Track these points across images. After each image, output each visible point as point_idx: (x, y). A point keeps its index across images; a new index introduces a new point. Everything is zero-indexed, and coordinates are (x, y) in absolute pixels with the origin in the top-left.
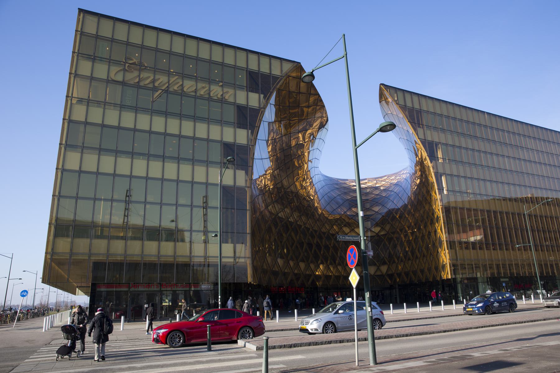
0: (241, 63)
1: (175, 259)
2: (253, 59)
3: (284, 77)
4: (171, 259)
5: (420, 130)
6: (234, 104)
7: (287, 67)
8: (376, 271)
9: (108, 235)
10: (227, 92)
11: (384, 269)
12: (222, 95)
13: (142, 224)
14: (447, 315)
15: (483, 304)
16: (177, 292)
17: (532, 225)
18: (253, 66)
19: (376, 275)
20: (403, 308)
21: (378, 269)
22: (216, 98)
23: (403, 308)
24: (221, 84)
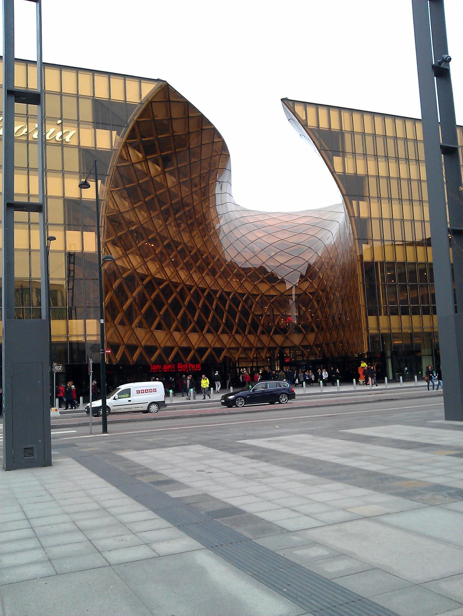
0: (85, 90)
1: (68, 339)
2: (101, 82)
3: (143, 104)
4: (64, 340)
5: (337, 160)
6: (79, 147)
7: (148, 89)
8: (302, 341)
9: (29, 287)
10: (68, 132)
11: (311, 337)
12: (62, 137)
13: (347, 151)
14: (120, 408)
15: (70, 404)
16: (93, 384)
17: (384, 290)
18: (101, 93)
19: (302, 346)
20: (383, 382)
21: (305, 338)
22: (53, 142)
23: (383, 382)
24: (59, 122)
